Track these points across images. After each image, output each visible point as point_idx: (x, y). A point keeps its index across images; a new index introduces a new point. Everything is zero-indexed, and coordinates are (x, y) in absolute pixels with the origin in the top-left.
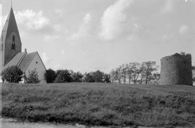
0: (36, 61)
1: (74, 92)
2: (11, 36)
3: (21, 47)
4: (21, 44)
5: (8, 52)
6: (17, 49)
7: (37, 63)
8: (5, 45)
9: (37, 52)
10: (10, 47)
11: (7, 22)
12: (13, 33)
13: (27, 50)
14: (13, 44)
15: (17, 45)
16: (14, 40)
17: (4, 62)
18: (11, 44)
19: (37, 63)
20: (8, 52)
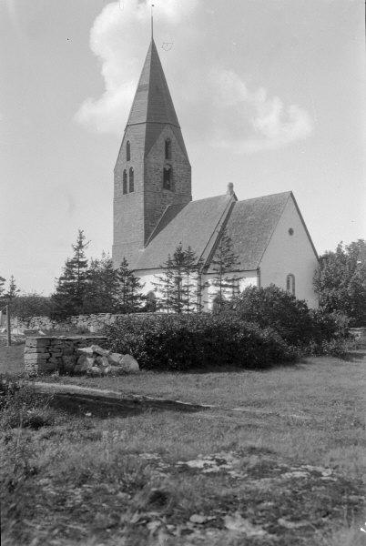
0: (288, 230)
1: (169, 398)
2: (161, 143)
3: (190, 182)
4: (189, 169)
5: (152, 195)
6: (178, 185)
7: (291, 232)
8: (143, 172)
9: (292, 194)
10: (158, 179)
11: (142, 93)
12: (167, 132)
13: (234, 189)
14: (168, 168)
15: (177, 172)
16: (168, 156)
17: (143, 232)
18: (161, 169)
19: (291, 232)
20: (152, 195)
